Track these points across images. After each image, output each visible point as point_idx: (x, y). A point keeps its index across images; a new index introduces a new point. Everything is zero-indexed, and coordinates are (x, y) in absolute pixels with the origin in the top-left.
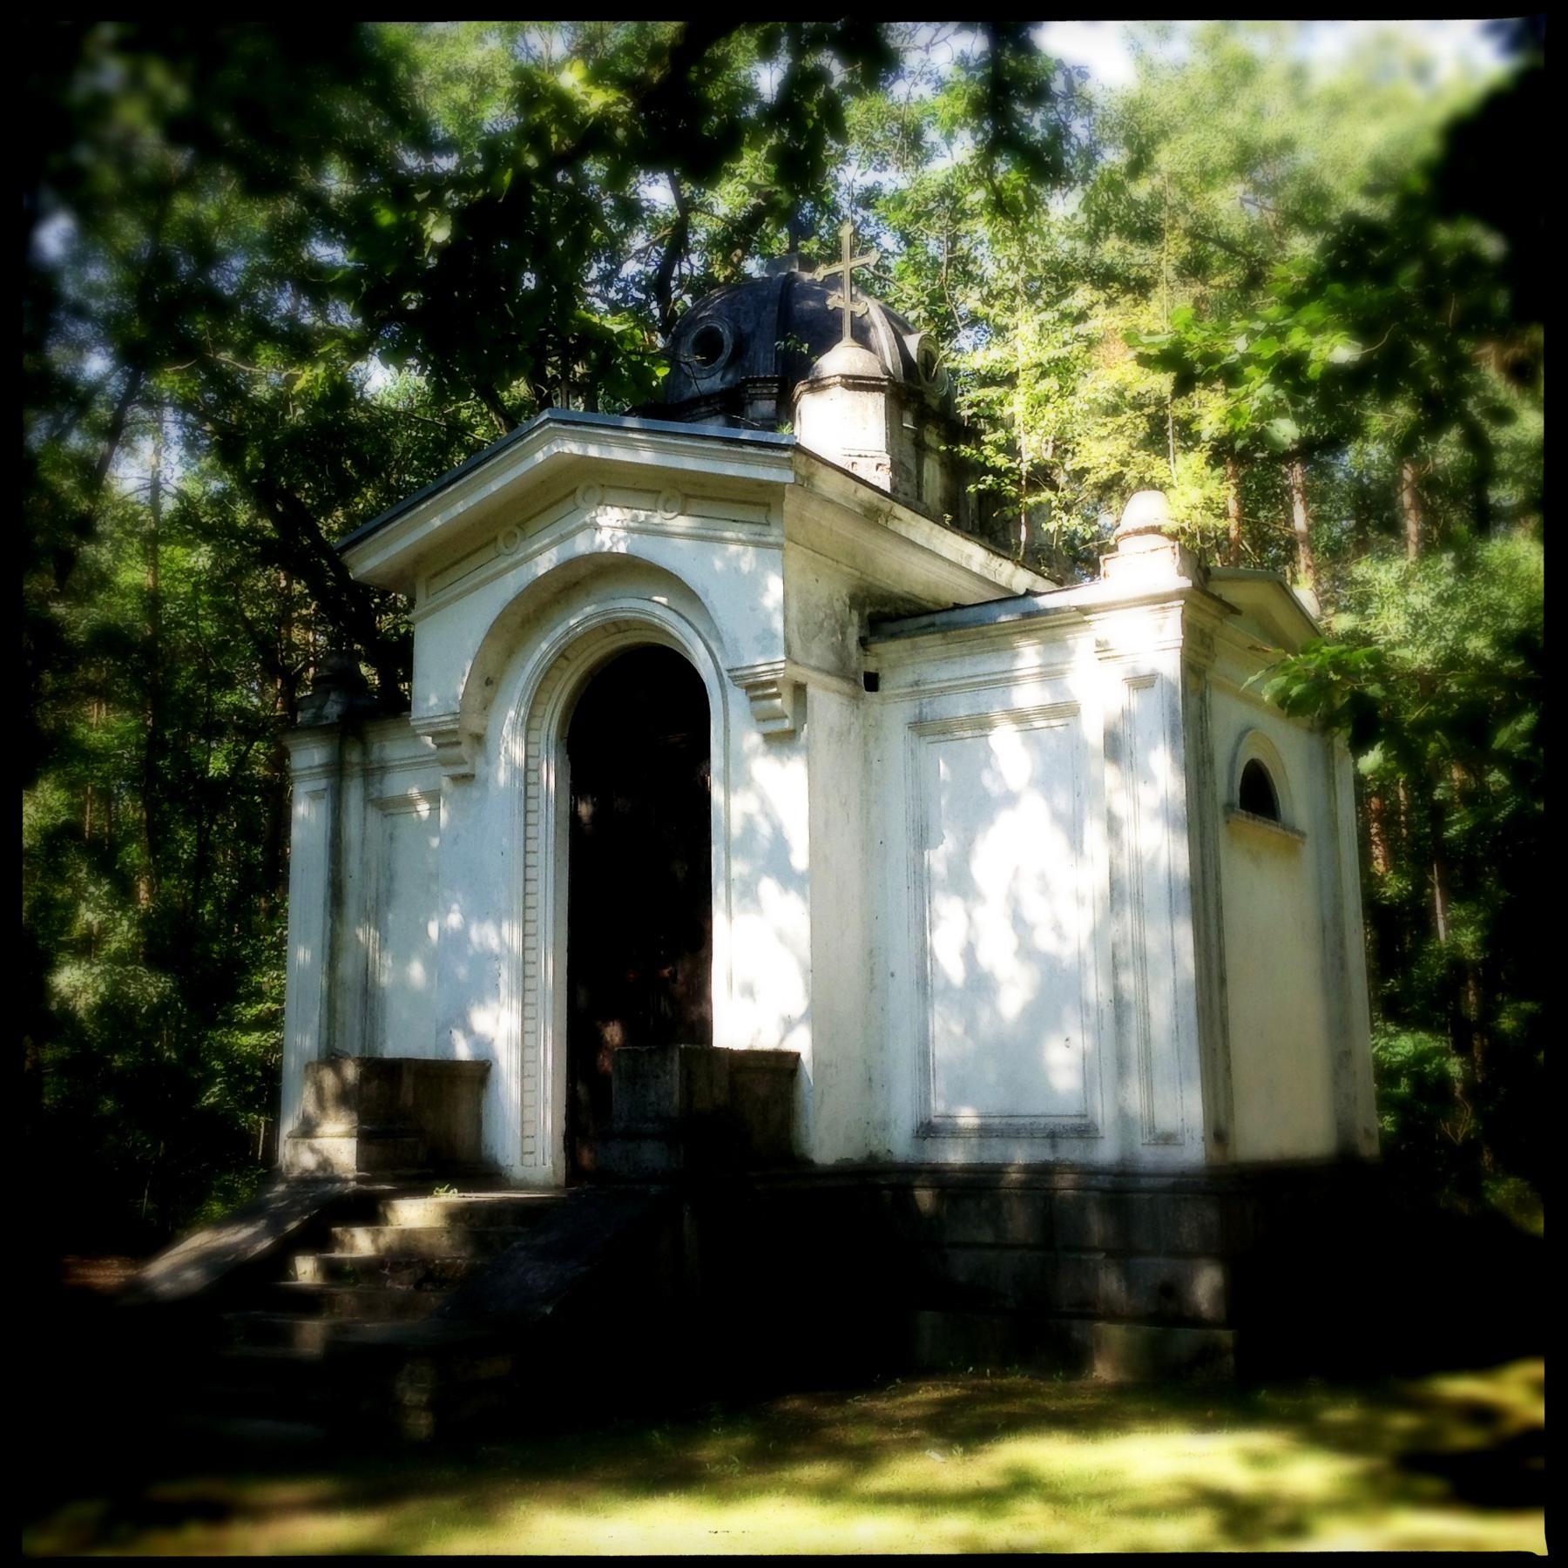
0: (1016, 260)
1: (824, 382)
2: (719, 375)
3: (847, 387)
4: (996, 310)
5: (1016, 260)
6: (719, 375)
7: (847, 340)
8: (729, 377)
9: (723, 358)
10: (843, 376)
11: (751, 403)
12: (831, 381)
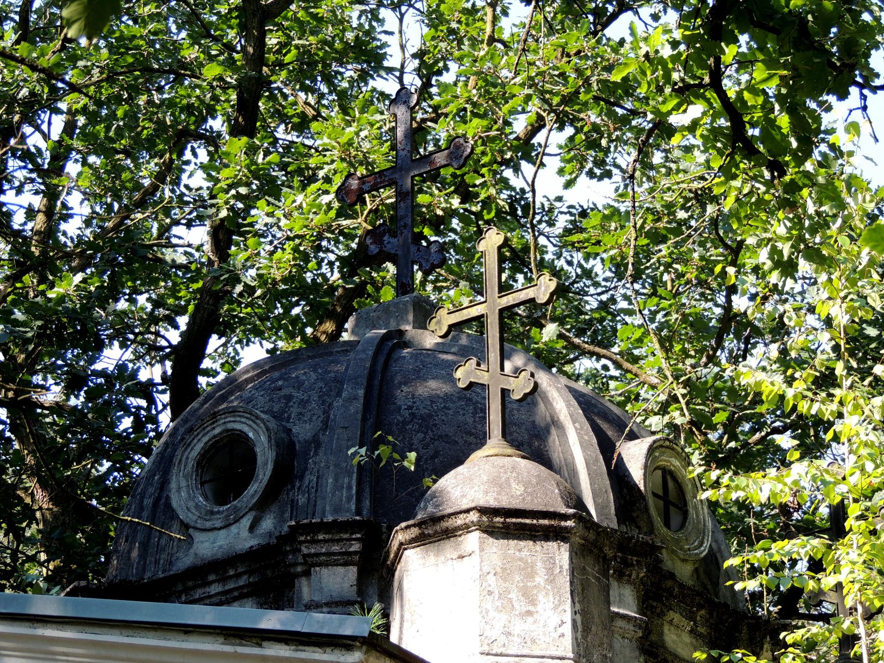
0: (786, 249)
1: (445, 524)
2: (246, 522)
3: (491, 531)
4: (799, 386)
5: (786, 249)
6: (246, 522)
7: (495, 443)
8: (268, 524)
9: (255, 488)
10: (483, 511)
11: (307, 574)
12: (459, 521)
